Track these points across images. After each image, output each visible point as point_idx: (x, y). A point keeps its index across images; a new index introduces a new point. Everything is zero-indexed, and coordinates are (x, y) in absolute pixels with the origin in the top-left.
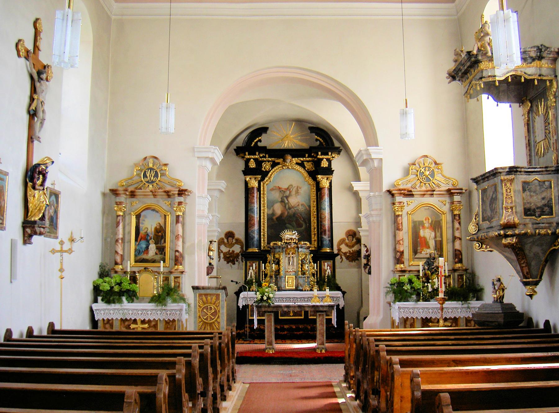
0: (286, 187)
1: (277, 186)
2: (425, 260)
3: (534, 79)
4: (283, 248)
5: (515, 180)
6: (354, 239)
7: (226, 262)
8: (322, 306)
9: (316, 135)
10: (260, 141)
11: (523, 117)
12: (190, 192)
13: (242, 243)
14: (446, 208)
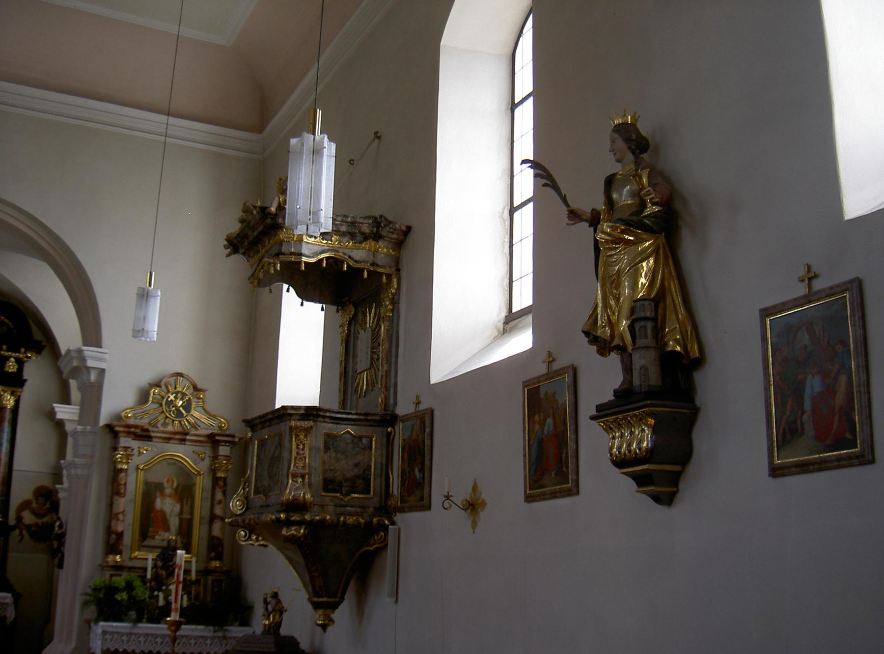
2: (160, 550)
3: (362, 270)
5: (314, 429)
6: (48, 503)
11: (341, 329)
14: (204, 466)
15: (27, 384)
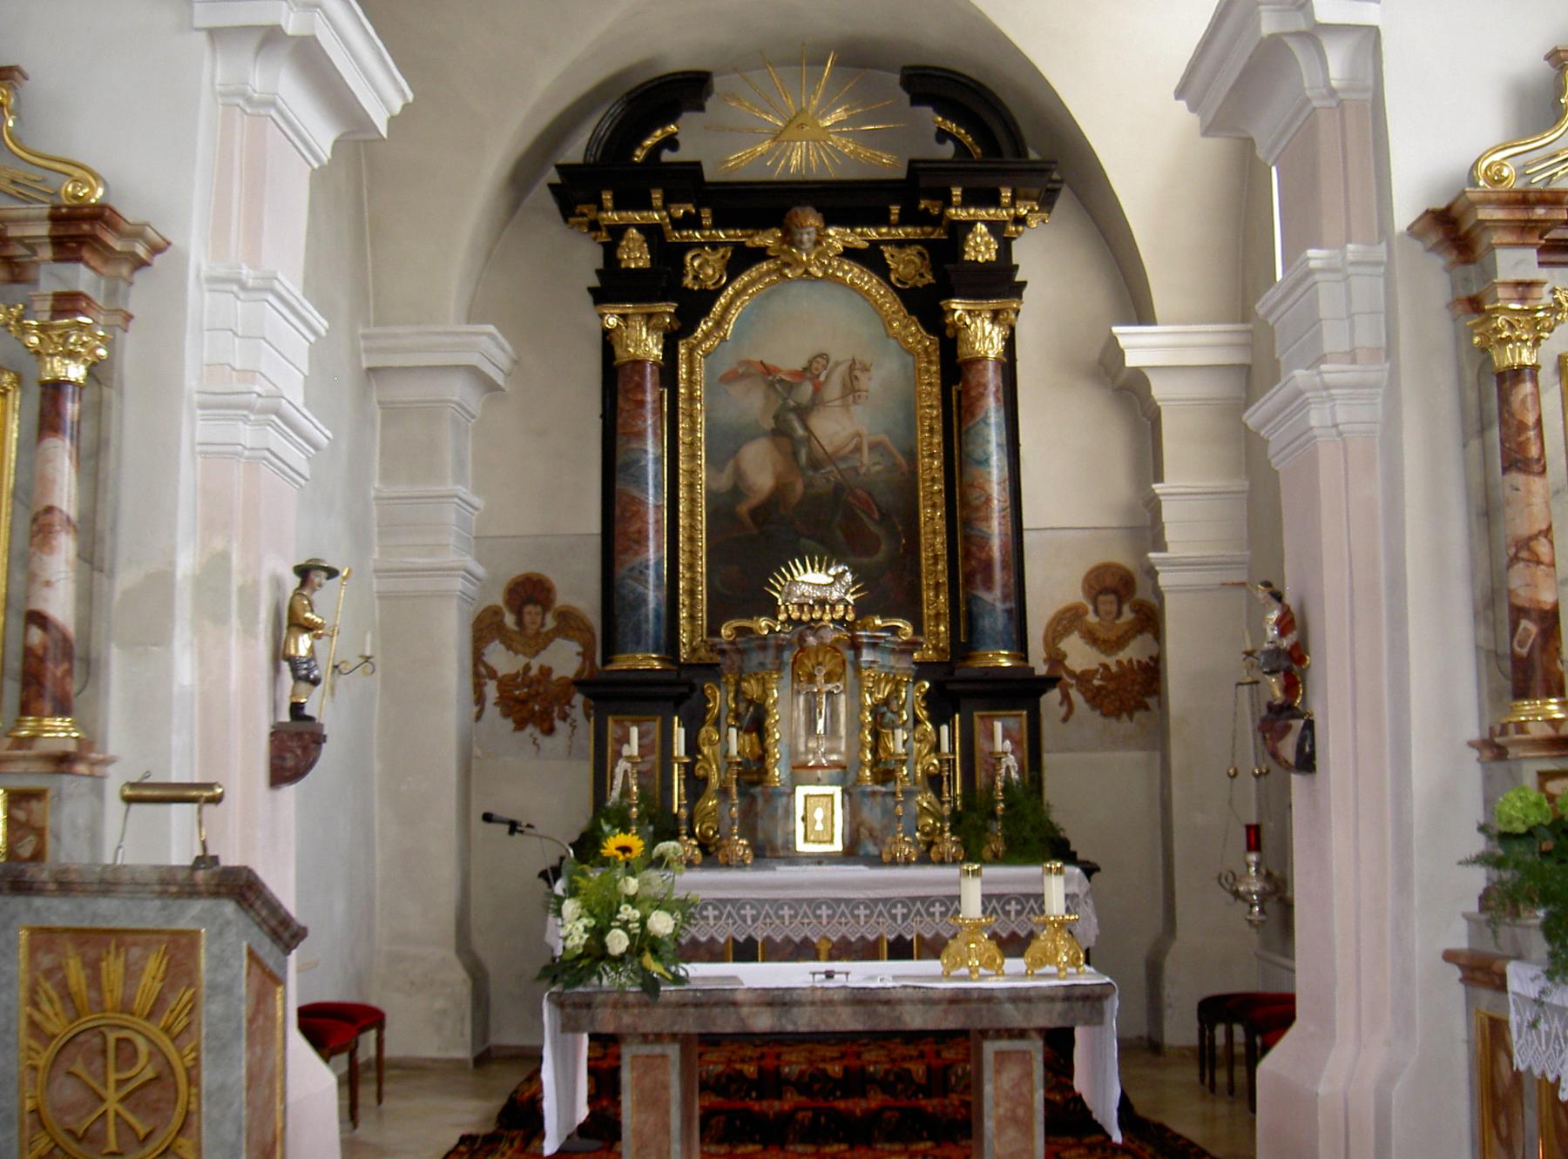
0: (799, 364)
1: (756, 358)
7: (509, 724)
8: (1018, 997)
9: (939, 112)
12: (138, 234)
13: (589, 629)
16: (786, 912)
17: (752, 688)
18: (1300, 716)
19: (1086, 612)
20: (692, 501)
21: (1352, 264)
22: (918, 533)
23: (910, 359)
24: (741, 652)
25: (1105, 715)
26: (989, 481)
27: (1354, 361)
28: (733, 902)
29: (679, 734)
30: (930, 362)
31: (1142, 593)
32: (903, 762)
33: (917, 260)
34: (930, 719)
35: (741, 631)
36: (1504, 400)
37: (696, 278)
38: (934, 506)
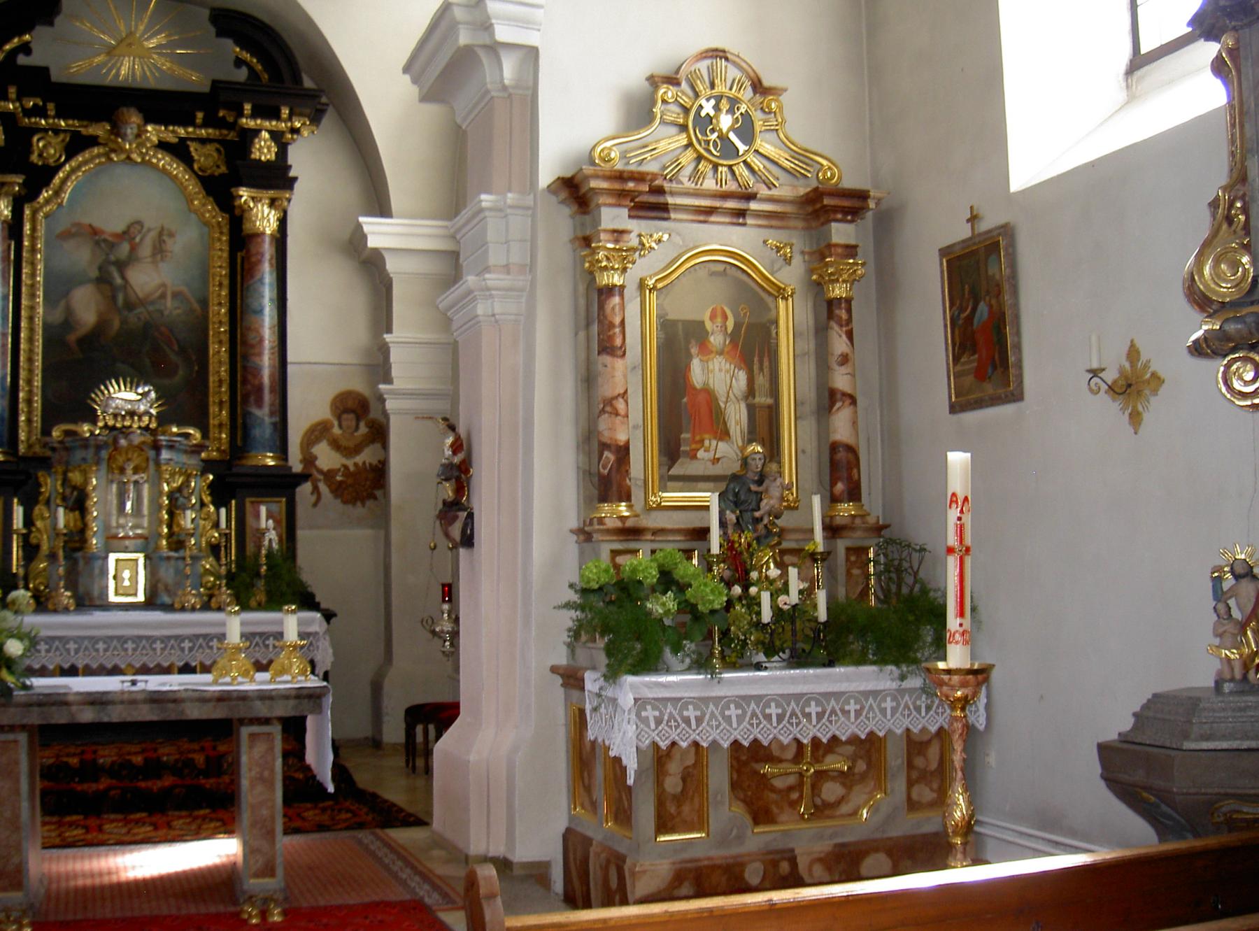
0: (119, 227)
1: (86, 220)
4: (99, 448)
8: (265, 696)
9: (237, 43)
10: (26, 49)
14: (792, 276)
15: (297, 186)
16: (101, 646)
17: (75, 477)
18: (465, 510)
19: (332, 426)
20: (31, 330)
21: (510, 207)
22: (207, 361)
23: (206, 229)
24: (67, 449)
25: (345, 502)
26: (262, 326)
27: (508, 273)
28: (60, 638)
29: (18, 513)
30: (221, 233)
31: (374, 414)
32: (192, 535)
33: (215, 154)
34: (213, 503)
35: (68, 433)
36: (601, 307)
37: (40, 155)
38: (220, 342)
